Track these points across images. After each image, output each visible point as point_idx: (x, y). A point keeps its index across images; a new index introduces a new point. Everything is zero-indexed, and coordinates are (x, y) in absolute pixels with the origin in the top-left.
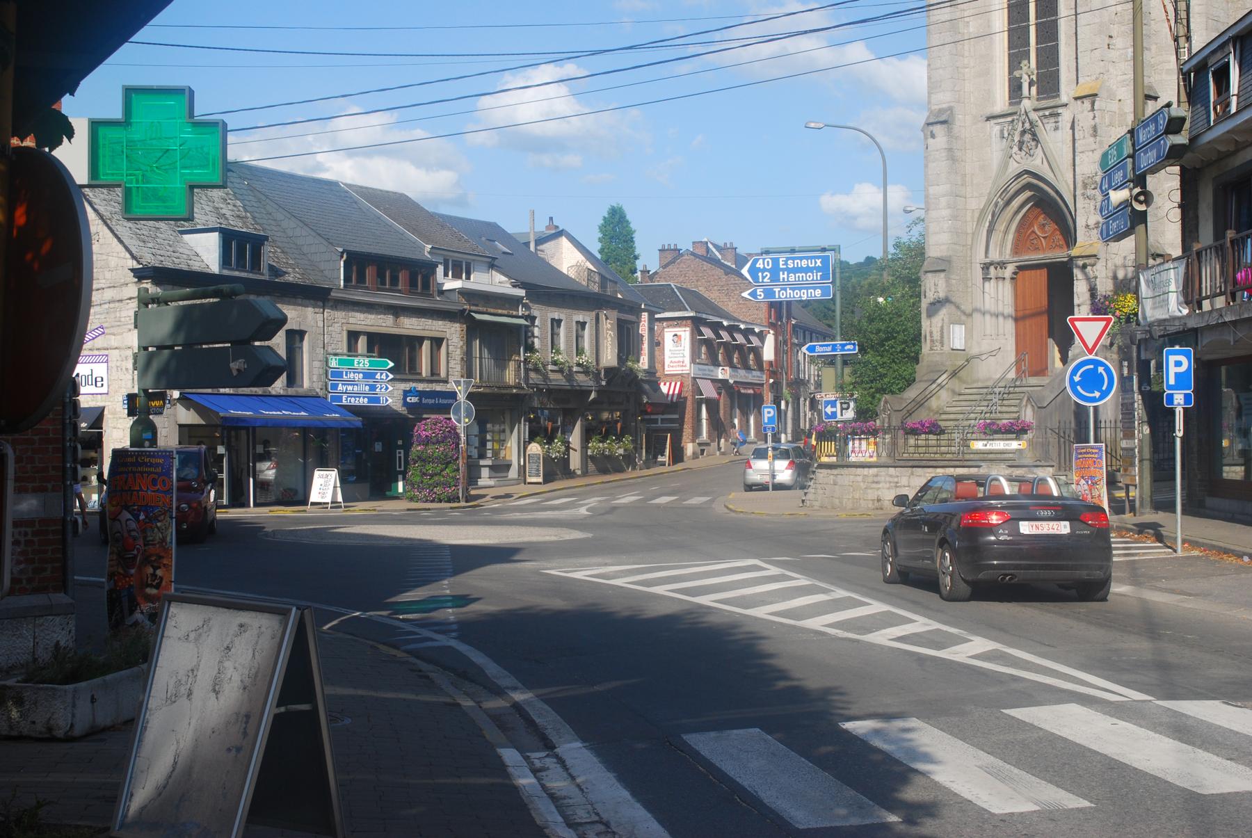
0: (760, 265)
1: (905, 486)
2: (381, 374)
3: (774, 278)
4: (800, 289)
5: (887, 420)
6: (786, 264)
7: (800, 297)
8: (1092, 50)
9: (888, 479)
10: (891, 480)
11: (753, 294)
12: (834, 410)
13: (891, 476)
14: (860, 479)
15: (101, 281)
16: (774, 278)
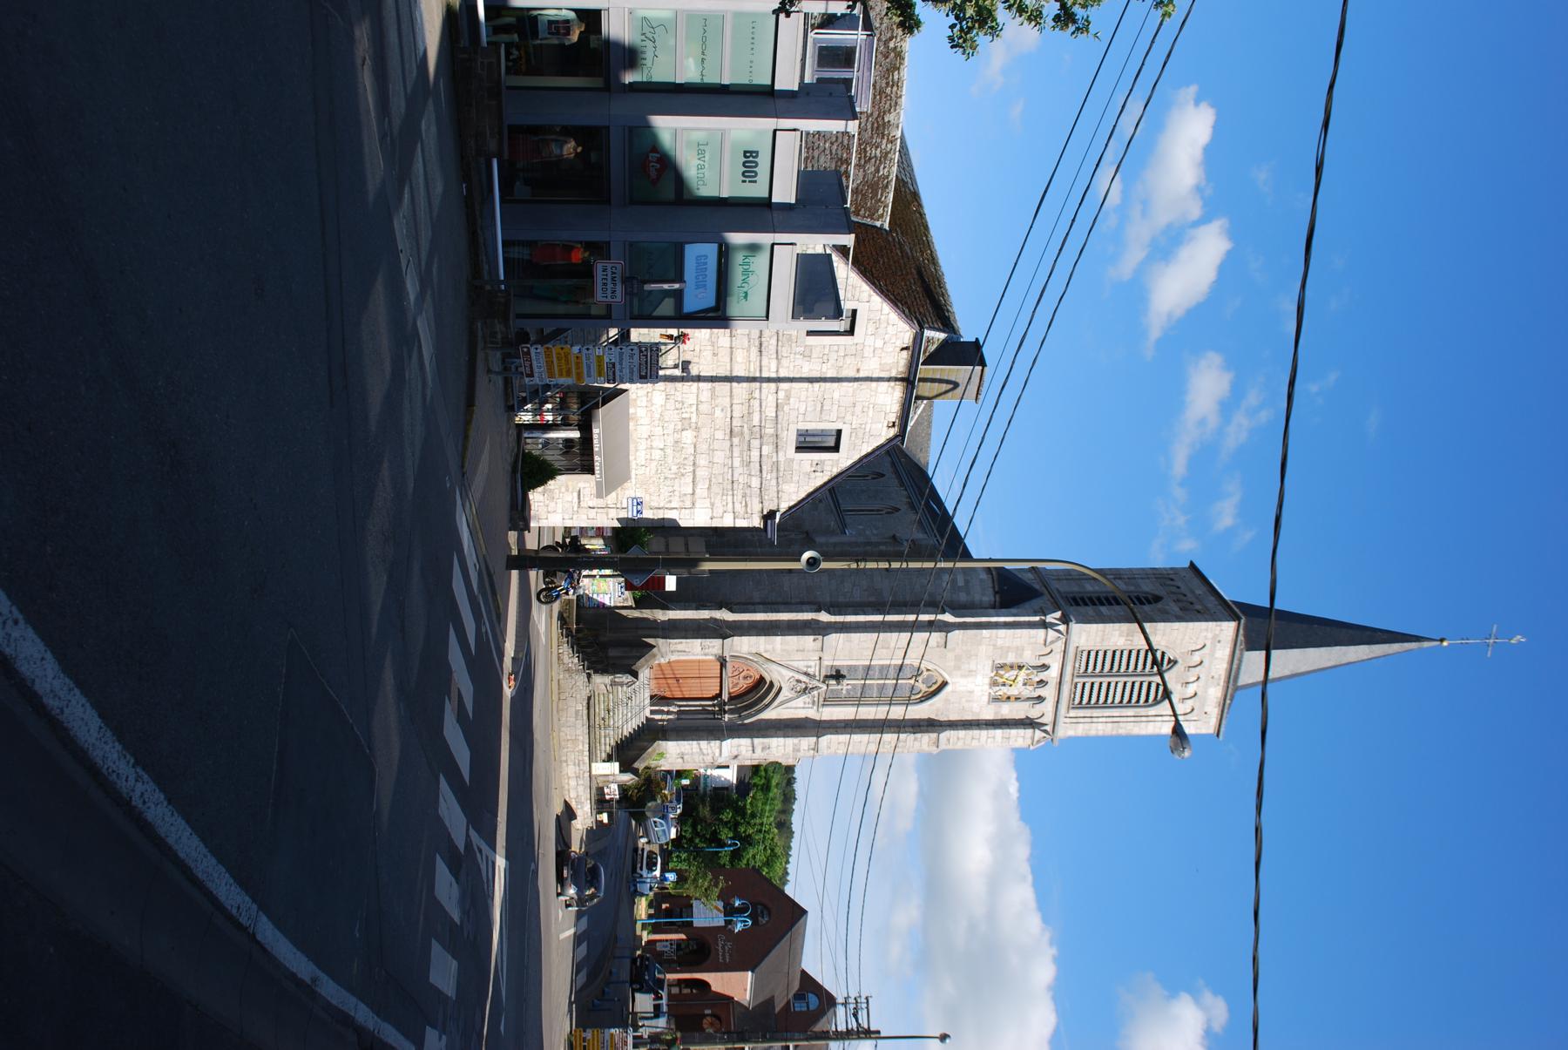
14: (581, 747)
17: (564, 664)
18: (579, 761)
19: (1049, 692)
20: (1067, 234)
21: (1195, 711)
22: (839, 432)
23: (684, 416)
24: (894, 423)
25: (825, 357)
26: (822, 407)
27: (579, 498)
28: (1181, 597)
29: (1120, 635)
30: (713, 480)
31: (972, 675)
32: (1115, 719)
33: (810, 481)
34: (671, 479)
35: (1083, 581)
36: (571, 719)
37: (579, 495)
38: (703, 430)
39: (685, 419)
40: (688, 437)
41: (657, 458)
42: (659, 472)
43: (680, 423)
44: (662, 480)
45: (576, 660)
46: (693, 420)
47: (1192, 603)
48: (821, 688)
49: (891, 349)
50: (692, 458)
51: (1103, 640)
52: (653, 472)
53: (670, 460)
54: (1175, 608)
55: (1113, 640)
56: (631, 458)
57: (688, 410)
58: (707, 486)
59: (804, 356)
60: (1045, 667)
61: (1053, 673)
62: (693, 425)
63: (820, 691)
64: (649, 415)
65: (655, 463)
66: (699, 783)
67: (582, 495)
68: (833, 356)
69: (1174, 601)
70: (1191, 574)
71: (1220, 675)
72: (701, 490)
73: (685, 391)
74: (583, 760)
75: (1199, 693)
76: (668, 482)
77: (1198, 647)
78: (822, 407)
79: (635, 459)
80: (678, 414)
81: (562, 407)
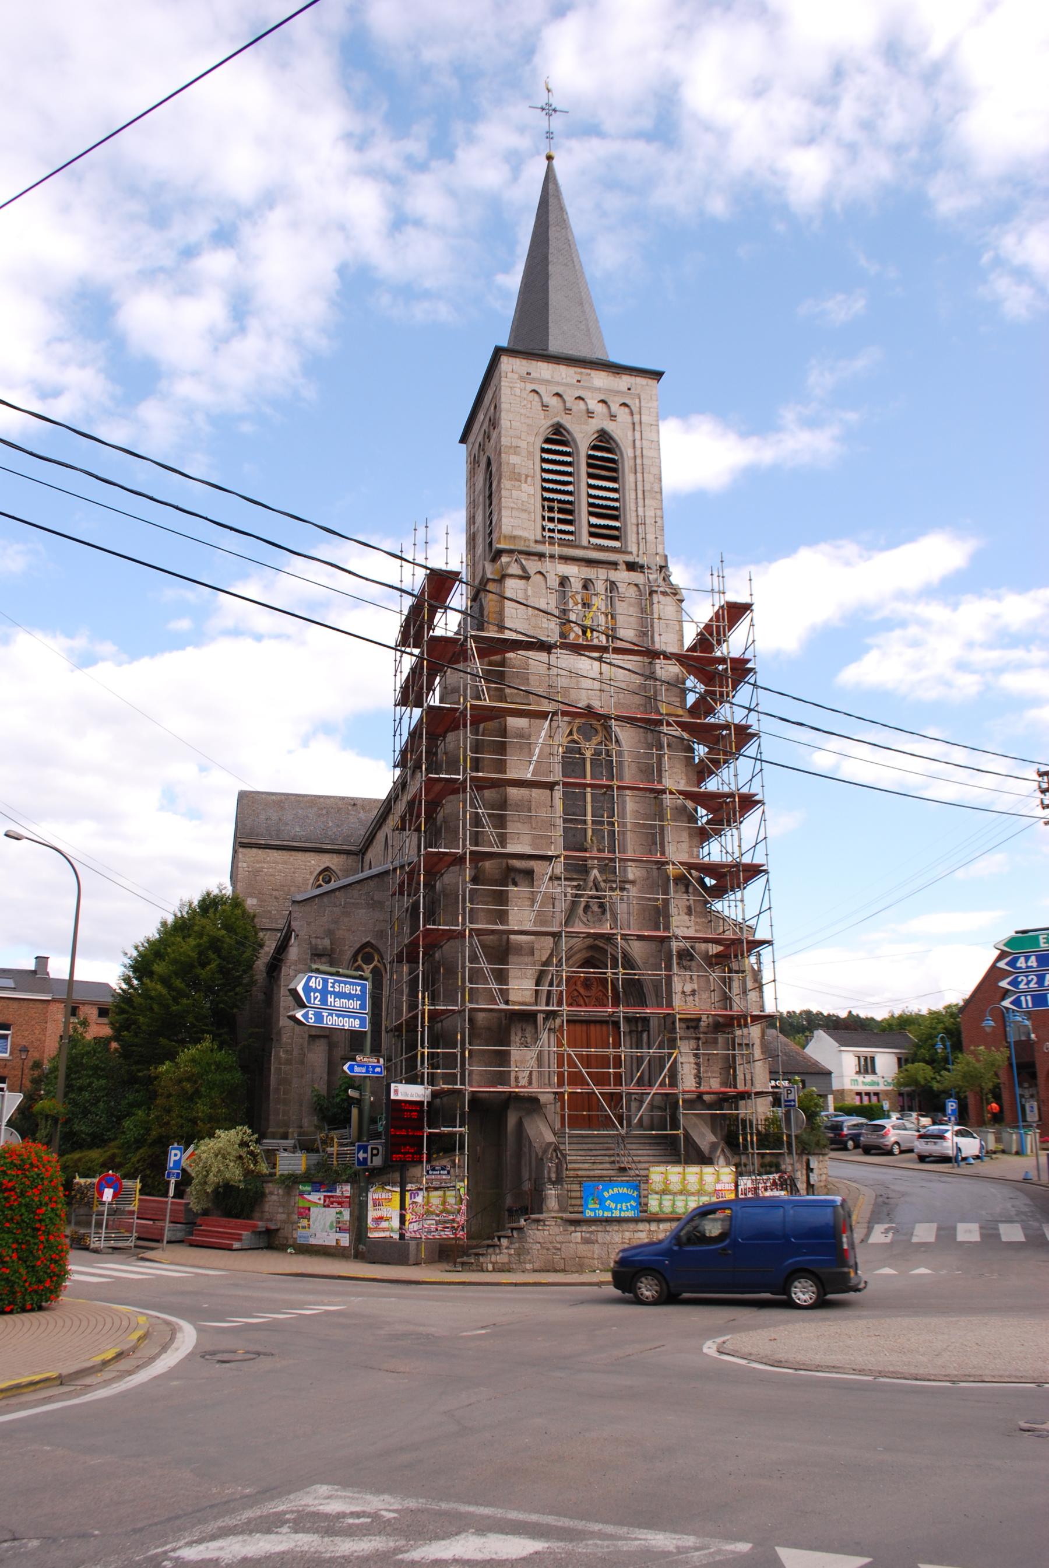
0: (312, 984)
2: (1027, 959)
3: (324, 1001)
4: (344, 1017)
5: (554, 1169)
6: (333, 987)
7: (343, 1026)
8: (678, 842)
11: (305, 1016)
12: (365, 1155)
16: (324, 1001)
17: (510, 1262)
19: (599, 575)
21: (627, 402)
32: (640, 495)
45: (504, 1242)
48: (595, 878)
61: (571, 570)
63: (600, 879)
70: (471, 439)
71: (575, 373)
75: (602, 397)
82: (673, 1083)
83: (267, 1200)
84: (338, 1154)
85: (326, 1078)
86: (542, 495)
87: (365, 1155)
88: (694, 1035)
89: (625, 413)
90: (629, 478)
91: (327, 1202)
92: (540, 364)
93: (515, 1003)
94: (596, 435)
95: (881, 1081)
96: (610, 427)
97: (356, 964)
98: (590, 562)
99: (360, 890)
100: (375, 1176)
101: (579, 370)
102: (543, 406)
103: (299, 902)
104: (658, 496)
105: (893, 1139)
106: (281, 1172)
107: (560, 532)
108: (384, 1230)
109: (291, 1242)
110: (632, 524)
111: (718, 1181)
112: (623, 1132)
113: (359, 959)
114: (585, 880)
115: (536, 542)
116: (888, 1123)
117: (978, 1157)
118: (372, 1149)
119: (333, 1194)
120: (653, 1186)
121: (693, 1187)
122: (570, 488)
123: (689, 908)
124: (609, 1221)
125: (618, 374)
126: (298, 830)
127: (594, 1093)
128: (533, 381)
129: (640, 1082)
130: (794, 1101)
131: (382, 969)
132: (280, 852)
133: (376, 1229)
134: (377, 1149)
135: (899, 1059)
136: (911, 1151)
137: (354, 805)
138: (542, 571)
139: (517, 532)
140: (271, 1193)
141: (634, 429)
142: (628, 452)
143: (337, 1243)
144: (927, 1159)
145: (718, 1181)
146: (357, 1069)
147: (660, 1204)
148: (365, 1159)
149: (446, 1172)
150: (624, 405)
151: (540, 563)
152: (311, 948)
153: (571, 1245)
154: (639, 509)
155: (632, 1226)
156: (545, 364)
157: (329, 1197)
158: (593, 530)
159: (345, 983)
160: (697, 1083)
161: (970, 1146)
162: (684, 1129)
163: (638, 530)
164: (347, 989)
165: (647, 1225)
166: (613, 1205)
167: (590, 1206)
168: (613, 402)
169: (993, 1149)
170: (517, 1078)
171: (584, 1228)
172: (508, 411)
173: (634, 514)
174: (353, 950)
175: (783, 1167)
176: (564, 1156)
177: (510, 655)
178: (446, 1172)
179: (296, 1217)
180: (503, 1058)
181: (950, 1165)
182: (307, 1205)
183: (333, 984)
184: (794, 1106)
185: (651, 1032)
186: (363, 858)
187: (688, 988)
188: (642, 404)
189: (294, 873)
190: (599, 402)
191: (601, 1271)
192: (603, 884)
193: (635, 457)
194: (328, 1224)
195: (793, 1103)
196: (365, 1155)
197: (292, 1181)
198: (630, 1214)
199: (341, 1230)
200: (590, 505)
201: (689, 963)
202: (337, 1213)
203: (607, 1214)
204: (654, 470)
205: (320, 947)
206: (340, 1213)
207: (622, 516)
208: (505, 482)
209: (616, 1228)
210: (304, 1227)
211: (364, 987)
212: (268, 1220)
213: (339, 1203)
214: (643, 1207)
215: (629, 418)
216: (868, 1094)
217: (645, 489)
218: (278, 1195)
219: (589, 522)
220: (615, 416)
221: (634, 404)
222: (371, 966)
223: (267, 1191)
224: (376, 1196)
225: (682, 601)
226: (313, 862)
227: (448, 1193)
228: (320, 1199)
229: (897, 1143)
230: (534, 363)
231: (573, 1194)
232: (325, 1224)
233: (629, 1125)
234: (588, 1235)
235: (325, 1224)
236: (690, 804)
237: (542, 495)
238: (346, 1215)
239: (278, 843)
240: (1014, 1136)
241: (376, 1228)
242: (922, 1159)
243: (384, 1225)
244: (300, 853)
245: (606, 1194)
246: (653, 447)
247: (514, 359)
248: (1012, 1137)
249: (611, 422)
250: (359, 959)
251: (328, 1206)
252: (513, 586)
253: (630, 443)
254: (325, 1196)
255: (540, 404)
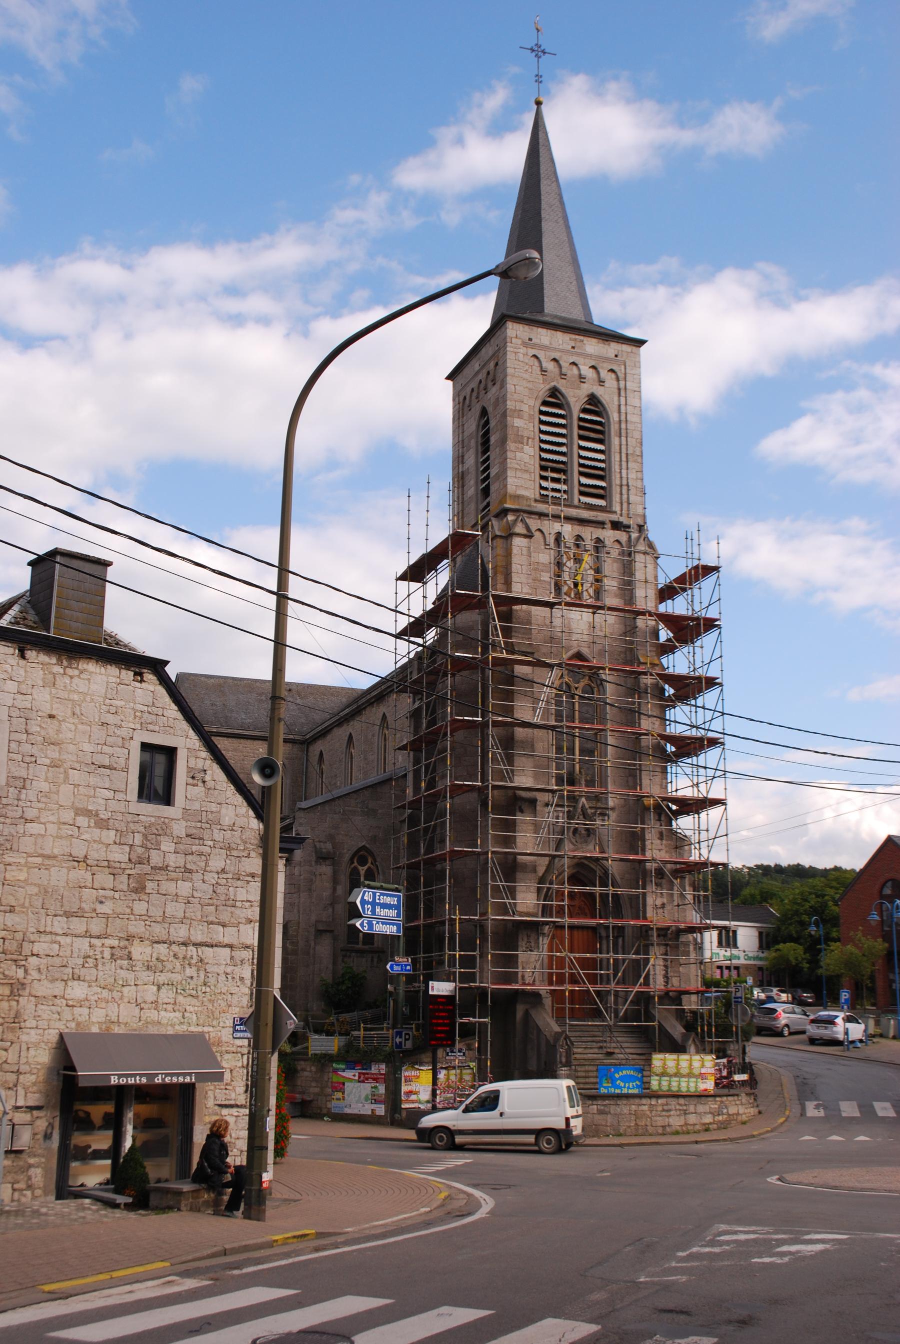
1: (692, 1113)
3: (373, 912)
5: (564, 1054)
6: (379, 899)
9: (678, 1107)
10: (681, 1108)
13: (680, 1105)
14: (645, 1108)
15: (206, 842)
16: (373, 912)
18: (664, 1110)
19: (589, 534)
20: (321, 610)
22: (145, 746)
23: (107, 954)
24: (136, 674)
25: (28, 759)
26: (104, 767)
27: (232, 1106)
28: (482, 386)
29: (522, 451)
30: (211, 919)
31: (569, 623)
32: (624, 459)
33: (218, 787)
34: (206, 976)
35: (465, 499)
36: (609, 1120)
37: (226, 1106)
38: (132, 929)
39: (112, 955)
40: (139, 951)
41: (172, 995)
42: (194, 992)
43: (118, 961)
44: (208, 989)
46: (115, 943)
47: (488, 373)
48: (583, 806)
49: (22, 672)
50: (175, 948)
51: (526, 471)
52: (194, 1001)
53: (177, 977)
54: (493, 391)
55: (526, 458)
56: (170, 1031)
57: (99, 949)
58: (221, 928)
59: (24, 787)
60: (558, 537)
61: (568, 530)
62: (123, 943)
63: (587, 806)
64: (103, 1005)
65: (180, 999)
66: (755, 965)
67: (227, 1102)
68: (26, 748)
69: (486, 393)
70: (461, 378)
71: (570, 339)
72: (220, 934)
73: (68, 953)
74: (663, 1105)
75: (593, 363)
76: (212, 981)
77: (536, 363)
78: (104, 767)
79: (173, 1025)
80: (103, 964)
81: (87, 1125)
82: (646, 983)
83: (298, 1075)
84: (364, 1037)
85: (331, 968)
86: (540, 456)
87: (400, 1040)
88: (664, 942)
89: (612, 379)
90: (615, 441)
91: (362, 1078)
92: (540, 330)
93: (521, 914)
94: (586, 399)
95: (742, 955)
96: (599, 391)
97: (353, 866)
98: (582, 522)
99: (356, 799)
100: (412, 1057)
101: (574, 336)
102: (542, 370)
103: (304, 809)
104: (639, 459)
105: (783, 1022)
106: (313, 1052)
107: (554, 490)
108: (413, 1102)
109: (325, 1111)
110: (616, 485)
111: (703, 1066)
112: (611, 1023)
113: (355, 861)
114: (575, 806)
115: (536, 501)
116: (779, 1007)
117: (861, 1041)
118: (406, 1034)
119: (368, 1071)
120: (655, 1070)
121: (685, 1071)
122: (564, 449)
123: (661, 834)
124: (620, 1097)
125: (607, 341)
126: (243, 716)
127: (589, 990)
128: (534, 346)
129: (623, 981)
130: (741, 998)
131: (375, 870)
132: (230, 740)
133: (408, 1101)
134: (408, 1034)
135: (760, 934)
136: (803, 1032)
137: (290, 690)
138: (541, 528)
139: (521, 492)
140: (304, 1070)
141: (619, 395)
142: (614, 417)
143: (372, 1112)
144: (817, 1042)
145: (703, 1066)
146: (395, 968)
147: (660, 1084)
148: (400, 1043)
149: (462, 1054)
150: (612, 371)
151: (539, 521)
152: (316, 852)
153: (589, 1115)
154: (623, 471)
155: (637, 1101)
156: (545, 330)
157: (364, 1074)
158: (582, 489)
159: (387, 895)
160: (665, 982)
161: (857, 1031)
162: (659, 1022)
163: (621, 491)
164: (388, 900)
165: (649, 1100)
166: (622, 1084)
167: (605, 1085)
168: (602, 368)
169: (873, 1033)
170: (523, 977)
171: (599, 1102)
172: (513, 376)
173: (618, 476)
174: (351, 853)
175: (729, 1052)
176: (572, 1043)
177: (514, 607)
178: (462, 1054)
179: (330, 1090)
180: (512, 961)
181: (841, 1048)
182: (341, 1080)
183: (379, 896)
184: (741, 1002)
185: (626, 938)
186: (308, 748)
187: (659, 902)
188: (628, 371)
189: (243, 760)
190: (590, 367)
191: (613, 1136)
192: (590, 811)
193: (620, 421)
194: (363, 1096)
195: (740, 1000)
196: (400, 1040)
197: (324, 1060)
198: (635, 1091)
199: (376, 1102)
200: (581, 465)
201: (660, 881)
202: (372, 1088)
203: (618, 1091)
204: (636, 435)
205: (324, 850)
206: (376, 1087)
207: (607, 476)
208: (510, 444)
209: (625, 1102)
210: (338, 1099)
211: (399, 897)
212: (303, 1093)
213: (374, 1079)
214: (646, 1085)
215: (615, 383)
216: (728, 968)
217: (629, 452)
218: (311, 1071)
219: (579, 482)
220: (604, 382)
221: (620, 370)
222: (366, 868)
223: (299, 1068)
224: (407, 1074)
225: (657, 558)
226: (261, 750)
227: (464, 1071)
228: (354, 1076)
229: (787, 1026)
230: (535, 328)
231: (591, 1074)
232: (360, 1096)
233: (616, 1016)
234: (602, 1108)
235: (360, 1096)
236: (662, 742)
237: (540, 456)
238: (382, 1089)
239: (229, 731)
240: (892, 1022)
241: (407, 1100)
242: (813, 1041)
243: (413, 1097)
244: (249, 741)
245: (617, 1076)
246: (636, 412)
247: (518, 325)
248: (889, 1022)
249: (600, 387)
250: (355, 861)
251: (363, 1082)
252: (519, 544)
253: (616, 408)
254: (359, 1073)
255: (539, 368)
